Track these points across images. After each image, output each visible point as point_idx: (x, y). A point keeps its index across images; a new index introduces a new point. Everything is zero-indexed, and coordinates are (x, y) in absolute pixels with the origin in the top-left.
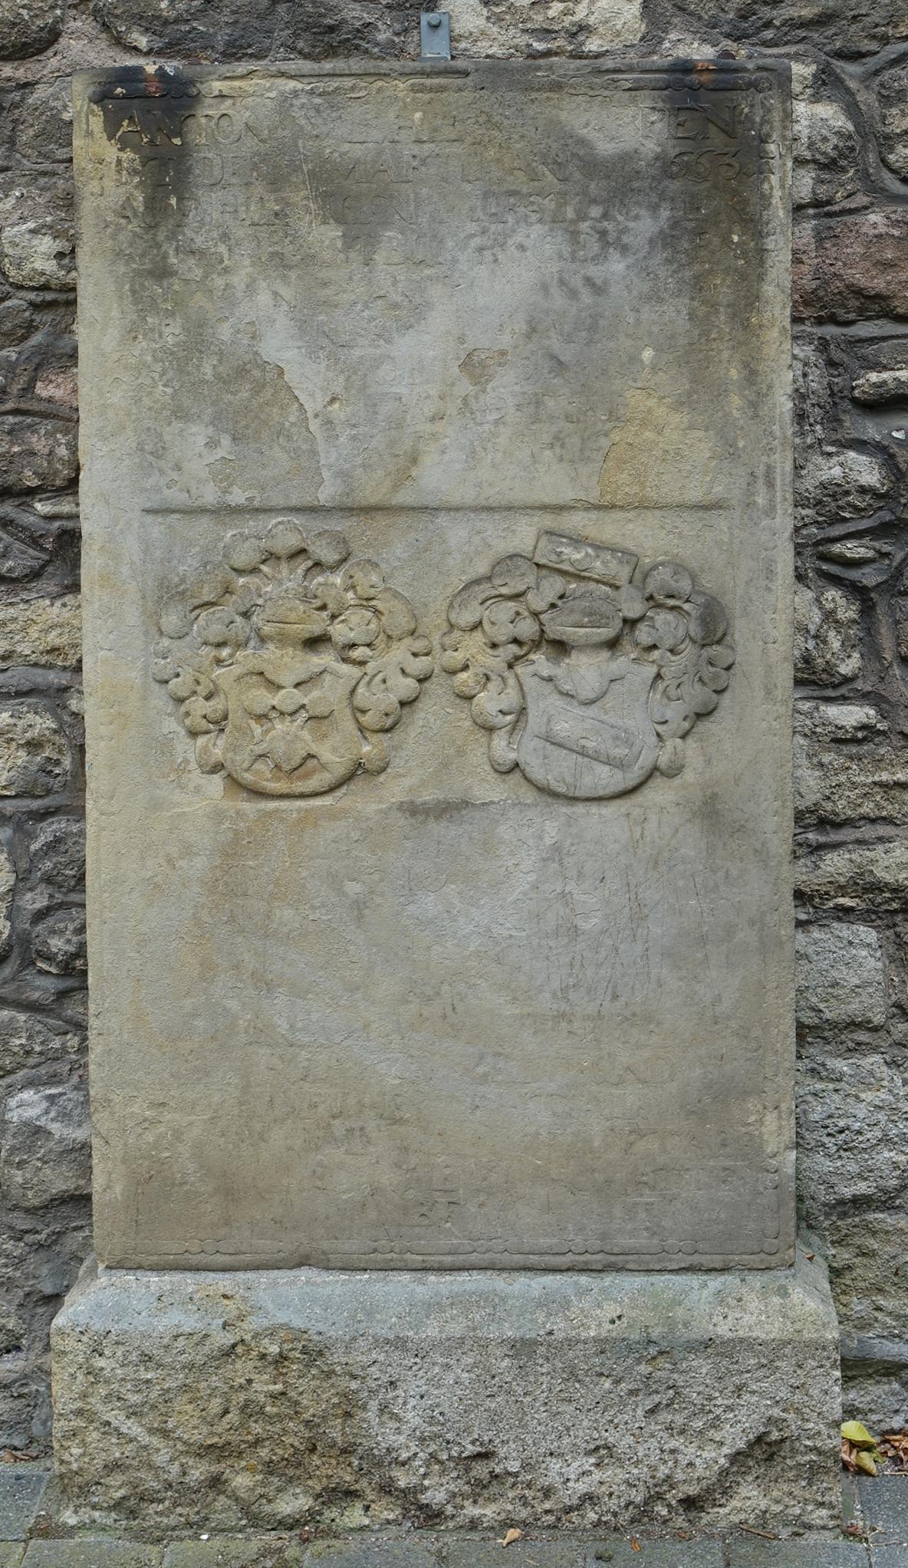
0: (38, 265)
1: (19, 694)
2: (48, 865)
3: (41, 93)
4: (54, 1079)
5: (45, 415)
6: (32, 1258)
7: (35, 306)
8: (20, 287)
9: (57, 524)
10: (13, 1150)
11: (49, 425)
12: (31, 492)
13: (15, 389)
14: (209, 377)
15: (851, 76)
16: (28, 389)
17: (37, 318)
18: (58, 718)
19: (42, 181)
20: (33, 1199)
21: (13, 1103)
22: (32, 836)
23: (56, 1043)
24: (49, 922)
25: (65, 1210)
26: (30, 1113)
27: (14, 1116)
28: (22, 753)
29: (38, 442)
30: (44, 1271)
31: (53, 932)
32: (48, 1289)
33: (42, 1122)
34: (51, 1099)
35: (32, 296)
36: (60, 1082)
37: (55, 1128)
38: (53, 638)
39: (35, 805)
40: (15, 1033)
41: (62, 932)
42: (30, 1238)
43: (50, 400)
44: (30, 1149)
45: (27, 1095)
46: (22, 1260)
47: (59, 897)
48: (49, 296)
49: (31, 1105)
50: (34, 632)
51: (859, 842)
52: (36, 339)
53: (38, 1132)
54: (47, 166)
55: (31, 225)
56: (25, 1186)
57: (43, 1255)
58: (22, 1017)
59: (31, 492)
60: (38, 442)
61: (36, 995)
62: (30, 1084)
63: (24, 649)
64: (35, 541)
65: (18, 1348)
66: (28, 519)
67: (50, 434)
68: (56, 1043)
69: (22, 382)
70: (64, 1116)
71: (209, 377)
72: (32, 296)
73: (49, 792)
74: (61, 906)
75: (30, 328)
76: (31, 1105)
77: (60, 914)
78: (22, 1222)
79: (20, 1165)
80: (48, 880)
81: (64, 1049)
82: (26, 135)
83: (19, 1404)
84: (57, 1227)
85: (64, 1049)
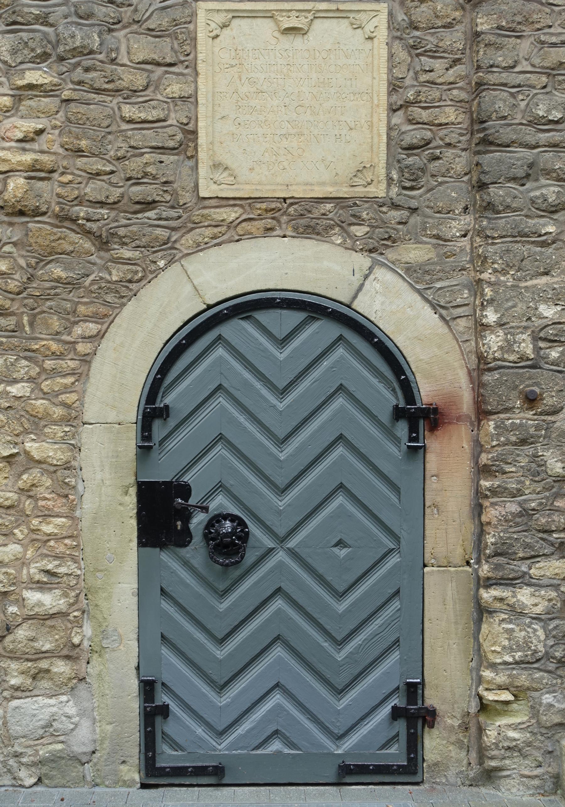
0: (558, 470)
1: (547, 586)
2: (554, 633)
3: (558, 424)
4: (554, 691)
5: (557, 511)
6: (546, 741)
7: (554, 481)
8: (550, 476)
9: (559, 540)
10: (544, 711)
11: (557, 513)
12: (553, 531)
13: (549, 504)
14: (16, 531)
15: (18, 309)
16: (552, 503)
17: (555, 484)
18: (558, 593)
19: (558, 448)
20: (548, 724)
21: (543, 698)
22: (549, 625)
23: (555, 682)
24: (554, 648)
25: (556, 728)
26: (549, 701)
27: (544, 701)
28: (546, 602)
29: (555, 518)
30: (549, 744)
31: (556, 651)
32: (550, 749)
33: (553, 703)
34: (555, 697)
35: (554, 478)
36: (556, 692)
37: (556, 704)
38: (557, 571)
39: (550, 616)
40: (544, 679)
41: (558, 651)
42: (546, 735)
43: (558, 507)
44: (548, 710)
45: (547, 696)
46: (543, 741)
47: (556, 642)
48: (559, 479)
49: (549, 698)
50: (551, 569)
51: (523, 723)
52: (554, 490)
53: (551, 706)
54: (559, 444)
55: (556, 459)
56: (546, 721)
57: (549, 740)
58: (545, 674)
59: (553, 531)
60: (555, 518)
61: (550, 668)
62: (547, 693)
63: (548, 574)
64: (552, 545)
65: (541, 766)
66: (551, 539)
67: (558, 516)
68: (555, 682)
69: (551, 501)
70: (558, 701)
71: (16, 531)
72: (554, 478)
73: (553, 613)
74: (556, 644)
75: (553, 487)
76: (549, 698)
77: (556, 646)
78: (544, 731)
79: (545, 715)
80: (554, 637)
81: (557, 683)
82: (554, 435)
83: (542, 781)
84: (553, 732)
85: (557, 683)
